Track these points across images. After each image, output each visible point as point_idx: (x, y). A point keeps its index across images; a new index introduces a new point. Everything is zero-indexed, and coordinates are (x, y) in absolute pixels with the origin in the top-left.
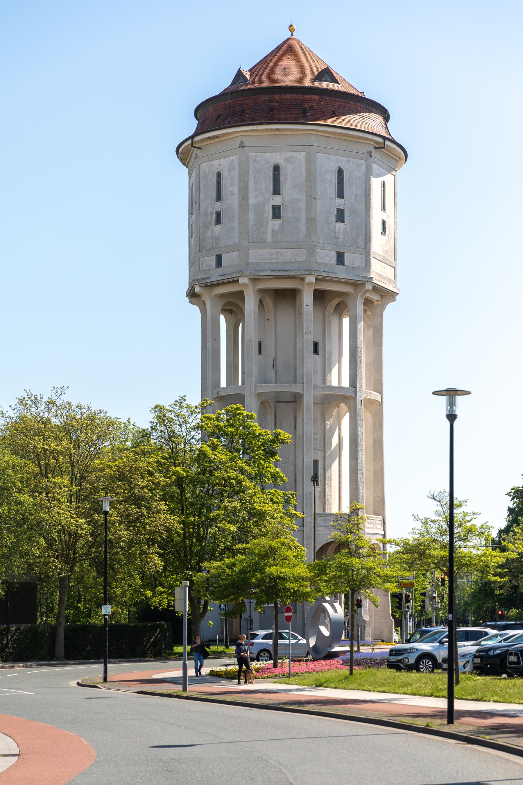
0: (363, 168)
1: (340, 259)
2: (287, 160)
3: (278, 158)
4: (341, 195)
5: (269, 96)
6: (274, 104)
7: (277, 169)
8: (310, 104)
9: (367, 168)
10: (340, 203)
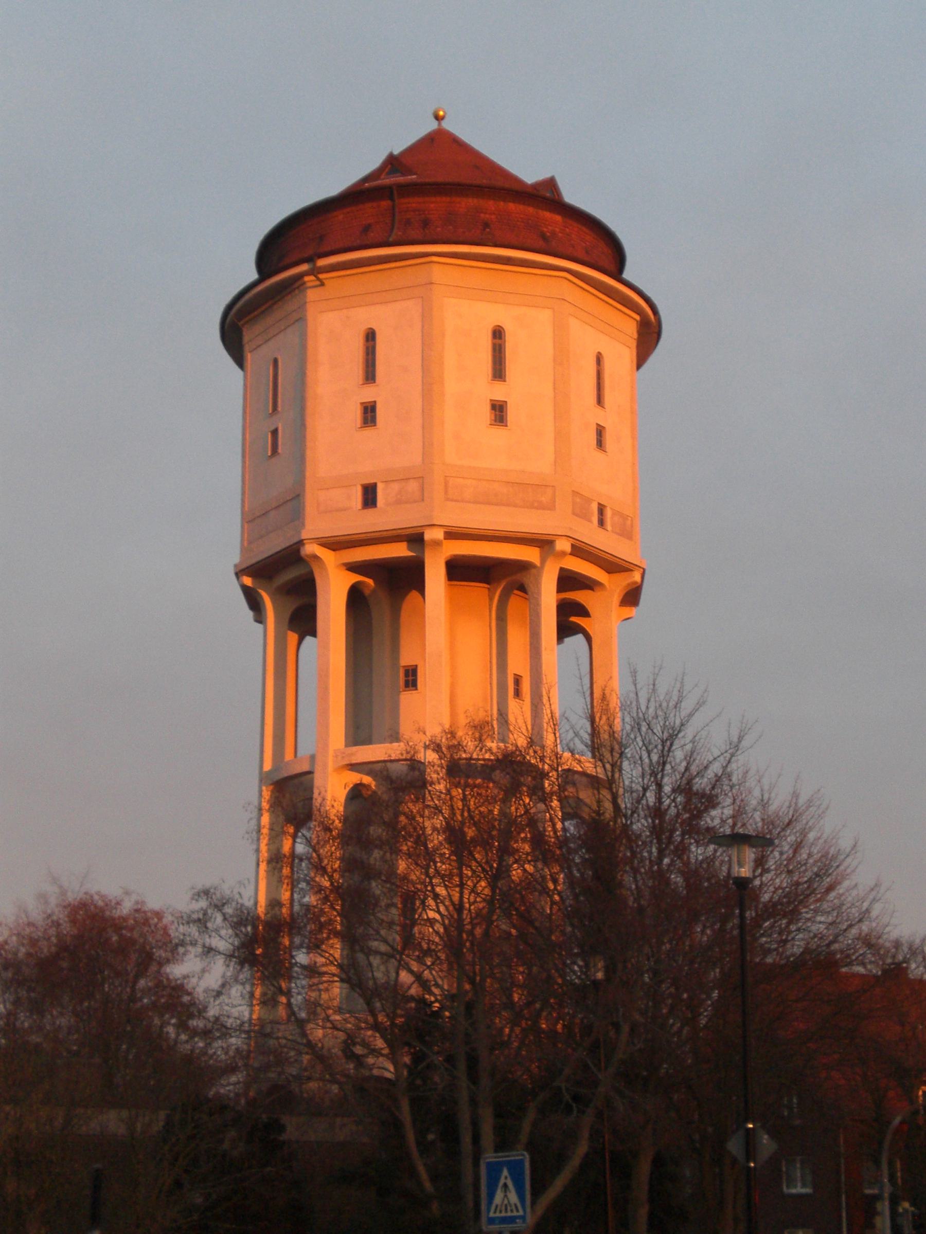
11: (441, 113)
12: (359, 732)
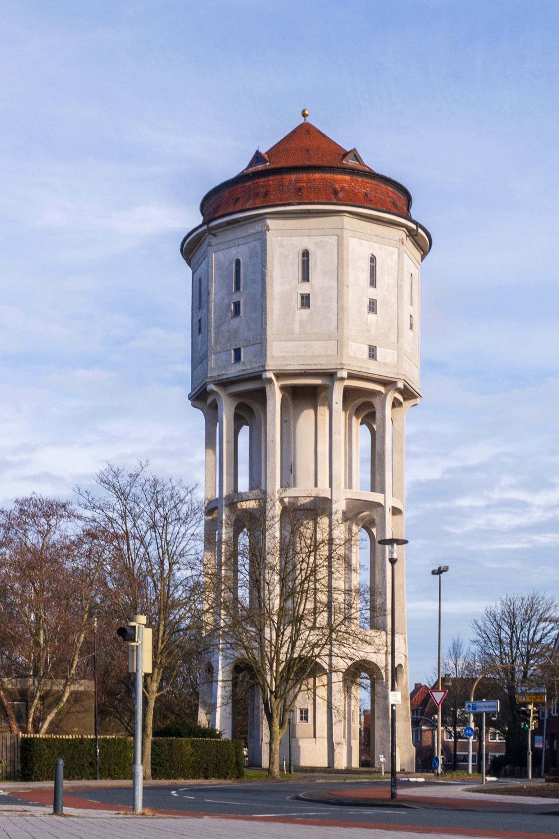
0: (395, 257)
1: (372, 353)
2: (317, 244)
3: (307, 243)
4: (373, 283)
5: (295, 176)
6: (301, 184)
7: (306, 254)
8: (341, 185)
9: (399, 256)
10: (372, 293)
11: (307, 112)
12: (285, 485)
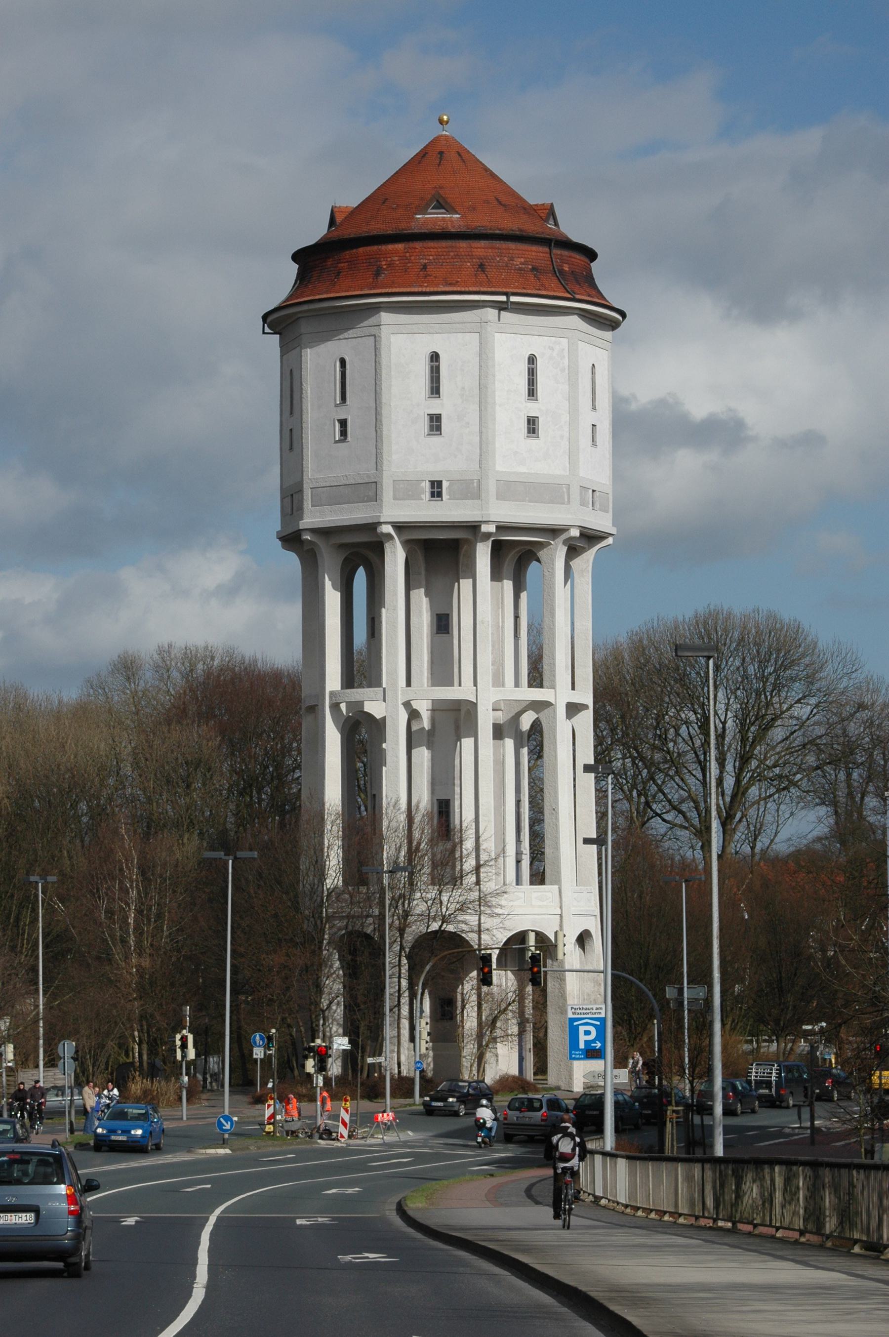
3: (437, 343)
